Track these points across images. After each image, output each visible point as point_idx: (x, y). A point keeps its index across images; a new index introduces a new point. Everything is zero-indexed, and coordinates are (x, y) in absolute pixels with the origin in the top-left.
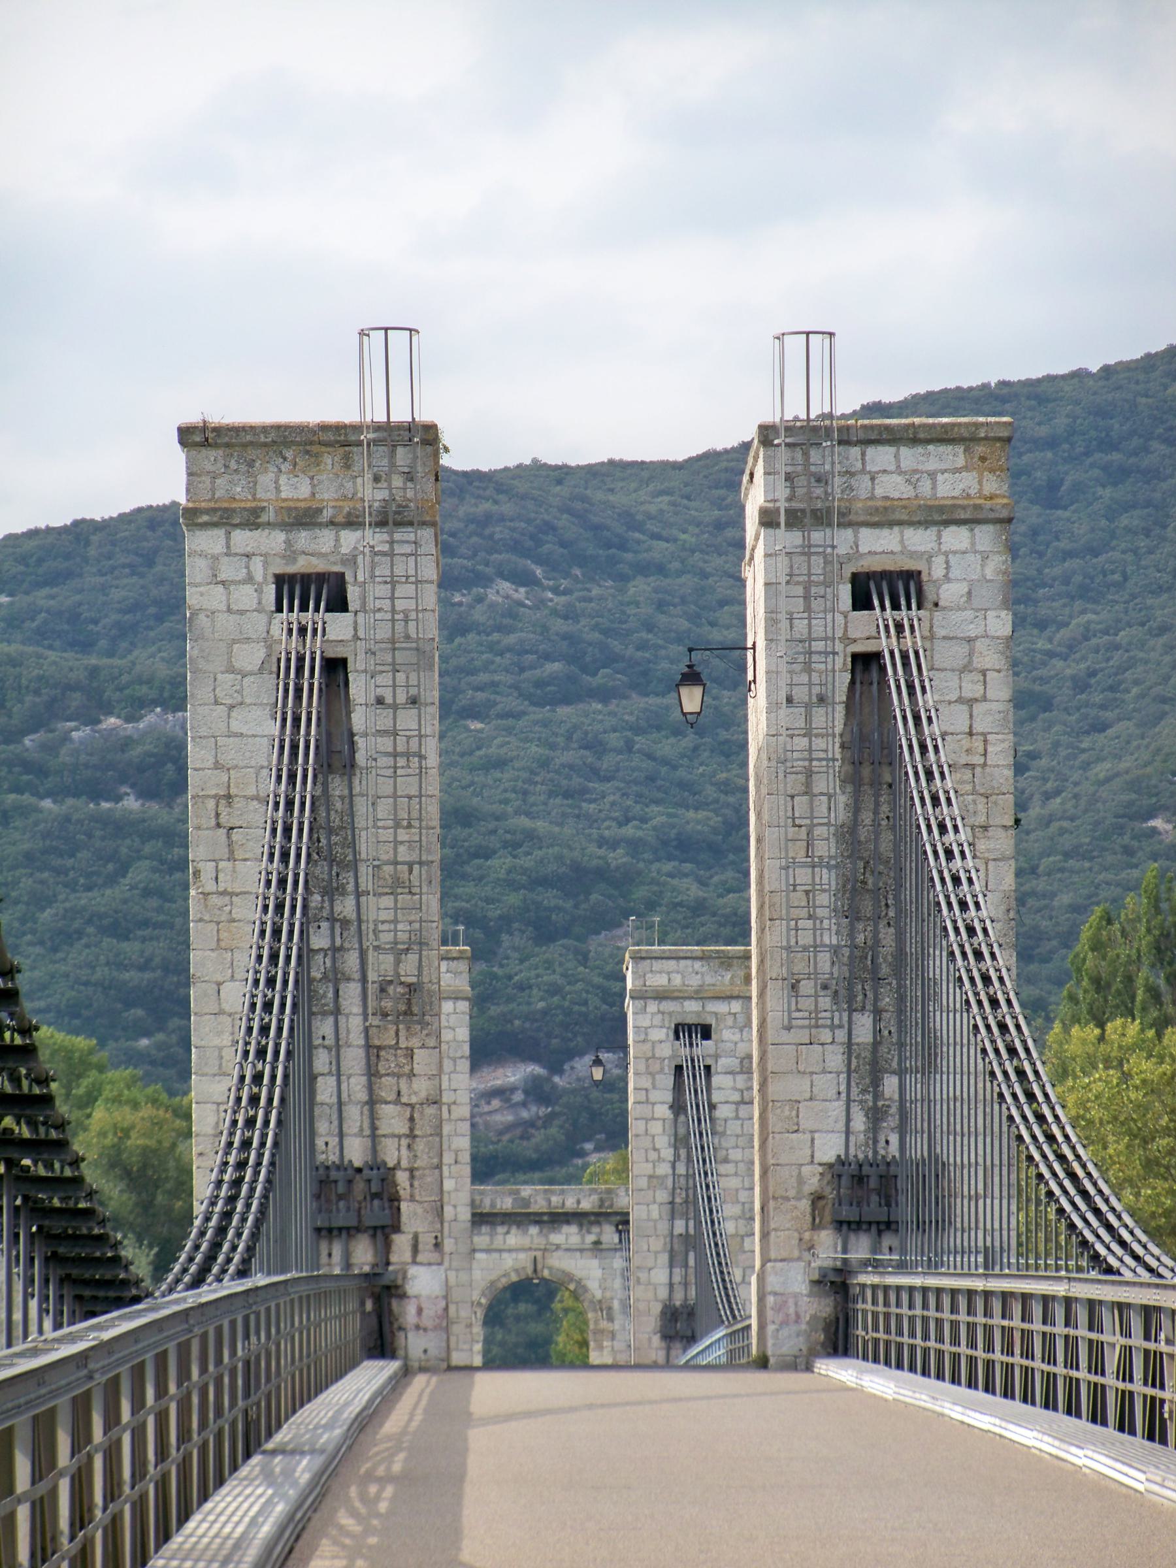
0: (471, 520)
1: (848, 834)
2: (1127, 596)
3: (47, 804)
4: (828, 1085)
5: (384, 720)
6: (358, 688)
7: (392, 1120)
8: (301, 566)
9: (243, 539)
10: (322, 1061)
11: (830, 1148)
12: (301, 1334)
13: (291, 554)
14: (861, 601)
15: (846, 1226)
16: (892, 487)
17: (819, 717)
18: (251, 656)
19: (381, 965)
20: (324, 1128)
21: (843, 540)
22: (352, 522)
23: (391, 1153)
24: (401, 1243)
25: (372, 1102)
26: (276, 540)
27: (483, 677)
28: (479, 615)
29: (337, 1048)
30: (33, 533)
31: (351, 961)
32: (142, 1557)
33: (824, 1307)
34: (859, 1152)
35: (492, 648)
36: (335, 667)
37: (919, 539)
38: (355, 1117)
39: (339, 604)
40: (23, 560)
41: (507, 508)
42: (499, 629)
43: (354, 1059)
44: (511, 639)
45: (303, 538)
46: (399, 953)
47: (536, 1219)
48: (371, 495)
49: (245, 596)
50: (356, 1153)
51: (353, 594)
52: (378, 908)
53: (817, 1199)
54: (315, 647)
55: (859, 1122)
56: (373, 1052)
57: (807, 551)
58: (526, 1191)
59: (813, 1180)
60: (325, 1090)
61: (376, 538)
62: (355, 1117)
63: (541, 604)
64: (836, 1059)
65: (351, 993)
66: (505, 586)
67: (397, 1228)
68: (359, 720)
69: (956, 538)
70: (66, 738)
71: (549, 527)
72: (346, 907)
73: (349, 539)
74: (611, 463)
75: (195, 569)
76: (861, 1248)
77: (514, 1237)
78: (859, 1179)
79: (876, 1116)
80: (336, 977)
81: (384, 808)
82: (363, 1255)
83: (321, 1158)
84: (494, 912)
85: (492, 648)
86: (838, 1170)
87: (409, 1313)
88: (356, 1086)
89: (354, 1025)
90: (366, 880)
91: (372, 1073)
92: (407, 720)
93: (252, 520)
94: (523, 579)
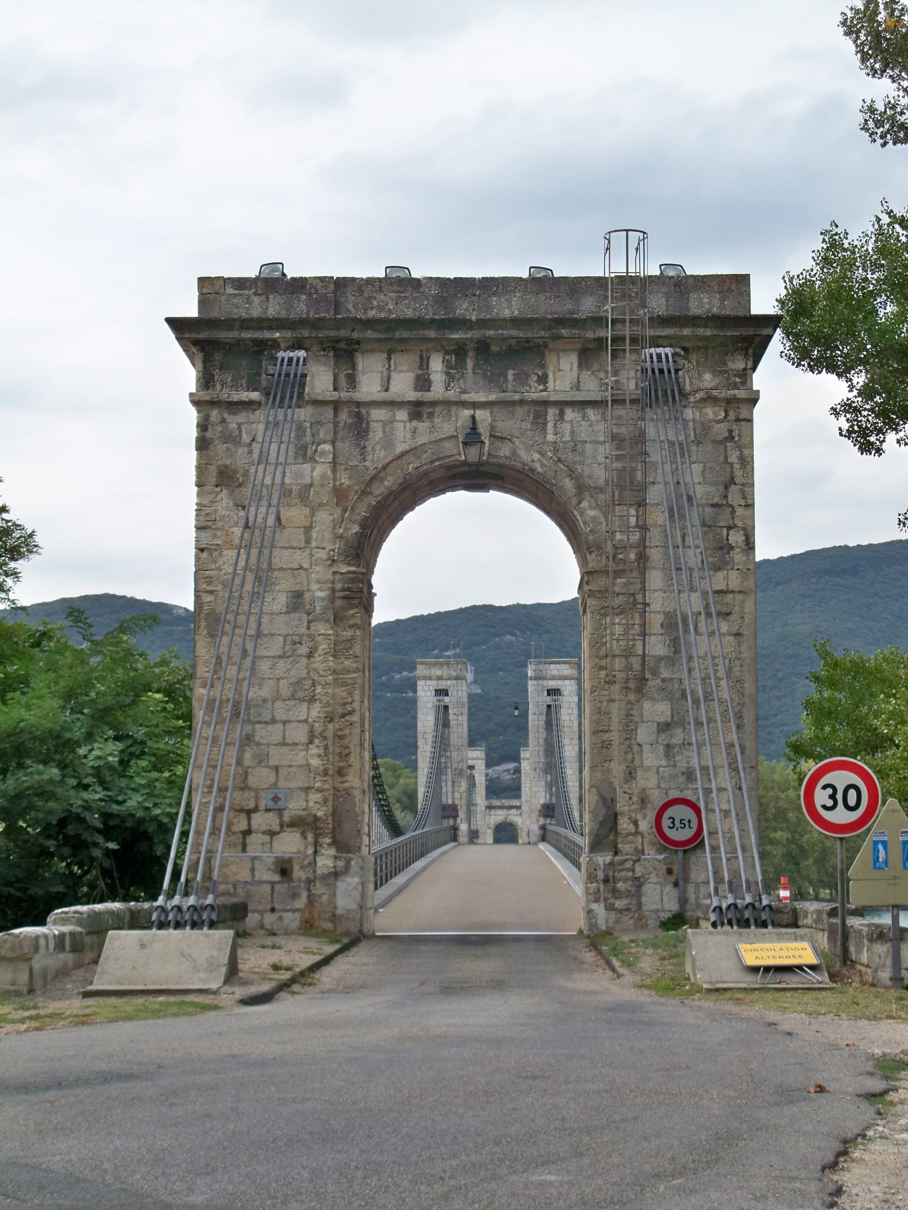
1: (546, 740)
9: (428, 682)
11: (542, 801)
16: (555, 672)
23: (457, 802)
26: (435, 682)
37: (560, 683)
38: (450, 795)
47: (506, 807)
69: (567, 682)
77: (500, 812)
94: (513, 634)
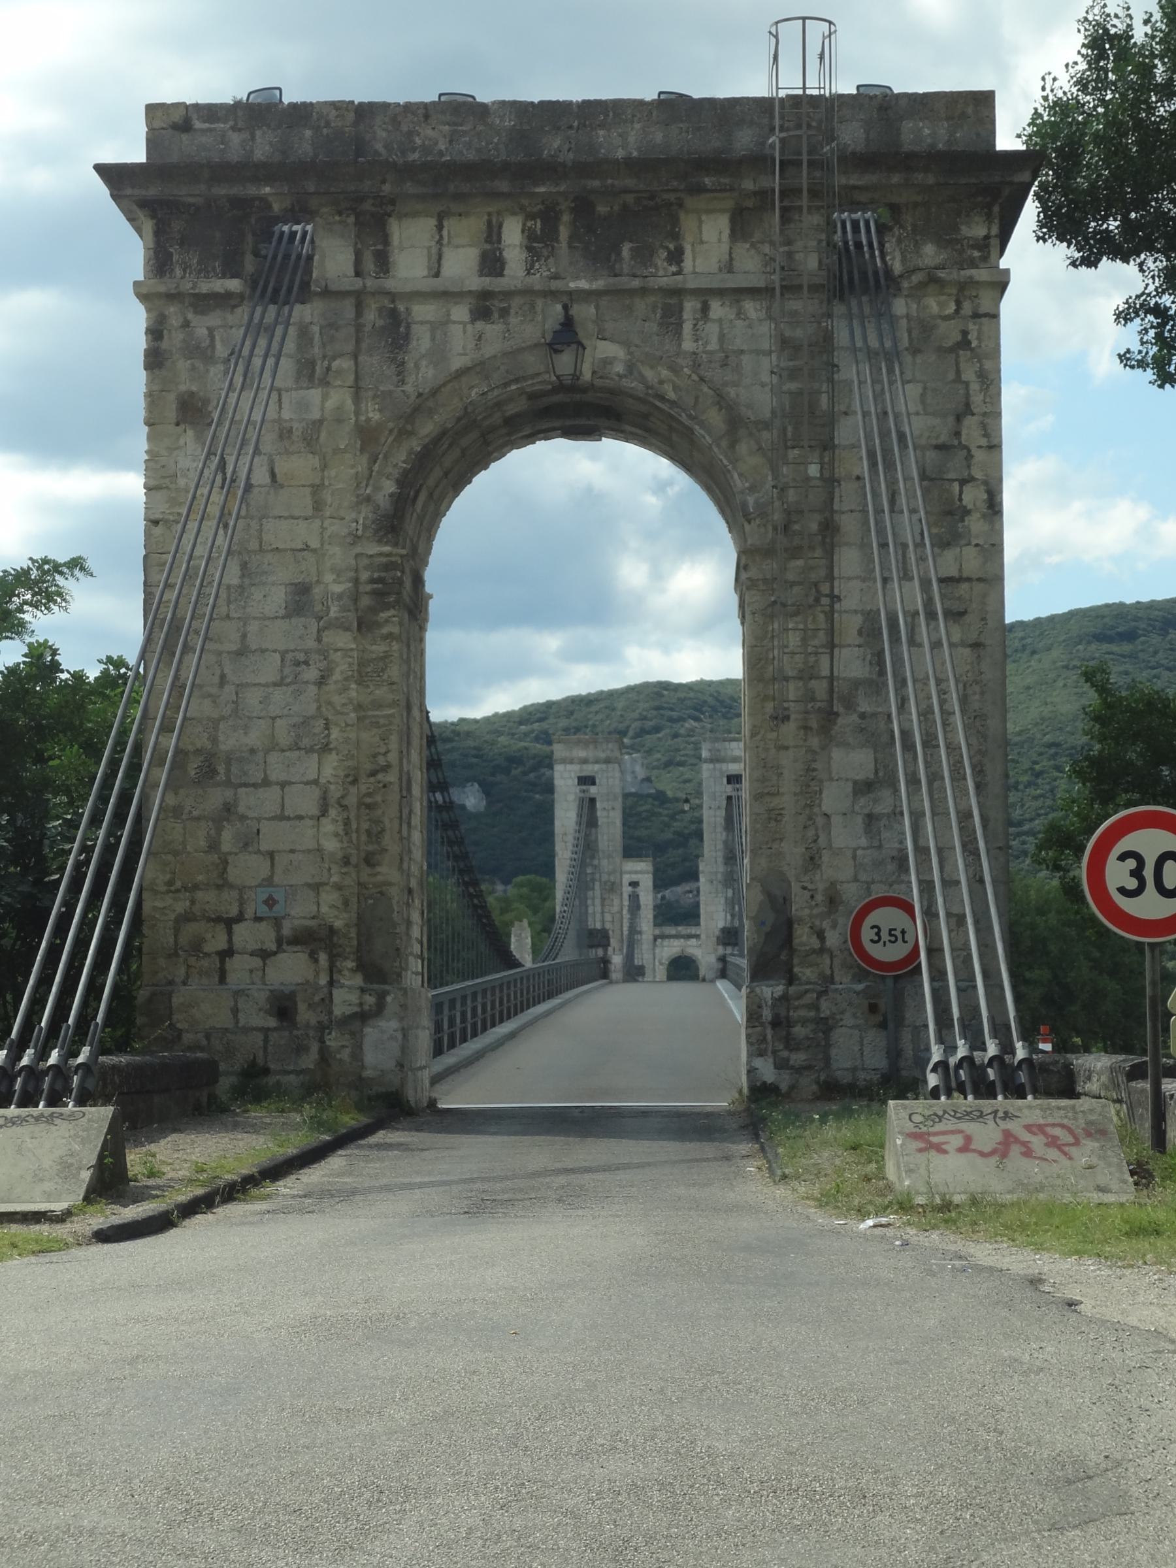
0: (678, 699)
1: (725, 842)
2: (641, 871)
3: (537, 796)
4: (721, 908)
5: (605, 813)
6: (598, 805)
7: (608, 917)
8: (584, 774)
9: (569, 767)
10: (589, 902)
11: (721, 924)
12: (85, 1019)
13: (581, 770)
14: (729, 782)
15: (725, 944)
17: (718, 813)
18: (571, 797)
19: (605, 877)
20: (590, 919)
21: (724, 766)
22: (597, 762)
23: (608, 926)
24: (610, 949)
25: (603, 913)
27: (682, 752)
28: (682, 731)
29: (593, 899)
30: (532, 705)
31: (597, 876)
32: (1172, 1341)
33: (720, 965)
34: (728, 925)
35: (687, 742)
36: (593, 801)
38: (598, 916)
39: (594, 783)
40: (530, 714)
41: (692, 695)
42: (689, 736)
43: (598, 902)
44: (693, 739)
45: (585, 767)
46: (609, 874)
47: (683, 937)
48: (603, 755)
49: (570, 782)
50: (598, 926)
51: (597, 781)
52: (604, 862)
53: (718, 938)
54: (587, 795)
55: (729, 917)
56: (603, 900)
57: (714, 769)
58: (680, 928)
59: (717, 933)
60: (590, 910)
61: (604, 766)
62: (598, 916)
63: (703, 727)
64: (723, 901)
65: (597, 885)
66: (692, 722)
67: (609, 945)
68: (599, 814)
70: (544, 774)
71: (705, 702)
72: (596, 862)
73: (597, 767)
74: (728, 680)
75: (557, 775)
76: (729, 950)
78: (729, 932)
79: (733, 916)
80: (593, 880)
81: (605, 837)
82: (600, 952)
83: (591, 925)
84: (686, 831)
85: (687, 742)
86: (724, 930)
87: (612, 967)
88: (598, 909)
89: (598, 893)
90: (601, 854)
91: (603, 905)
92: (612, 814)
93: (571, 762)
94: (697, 719)
